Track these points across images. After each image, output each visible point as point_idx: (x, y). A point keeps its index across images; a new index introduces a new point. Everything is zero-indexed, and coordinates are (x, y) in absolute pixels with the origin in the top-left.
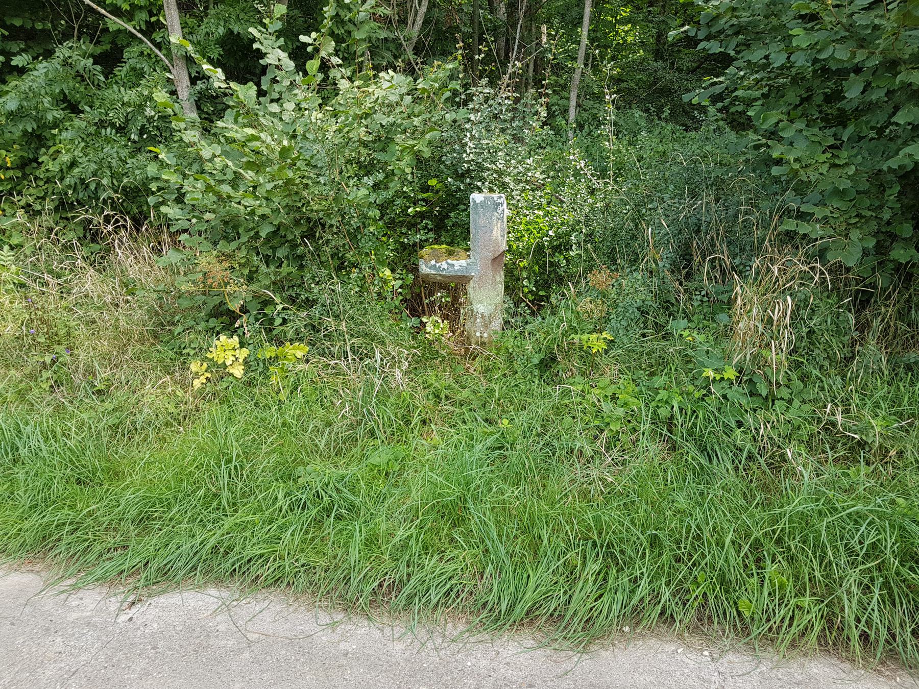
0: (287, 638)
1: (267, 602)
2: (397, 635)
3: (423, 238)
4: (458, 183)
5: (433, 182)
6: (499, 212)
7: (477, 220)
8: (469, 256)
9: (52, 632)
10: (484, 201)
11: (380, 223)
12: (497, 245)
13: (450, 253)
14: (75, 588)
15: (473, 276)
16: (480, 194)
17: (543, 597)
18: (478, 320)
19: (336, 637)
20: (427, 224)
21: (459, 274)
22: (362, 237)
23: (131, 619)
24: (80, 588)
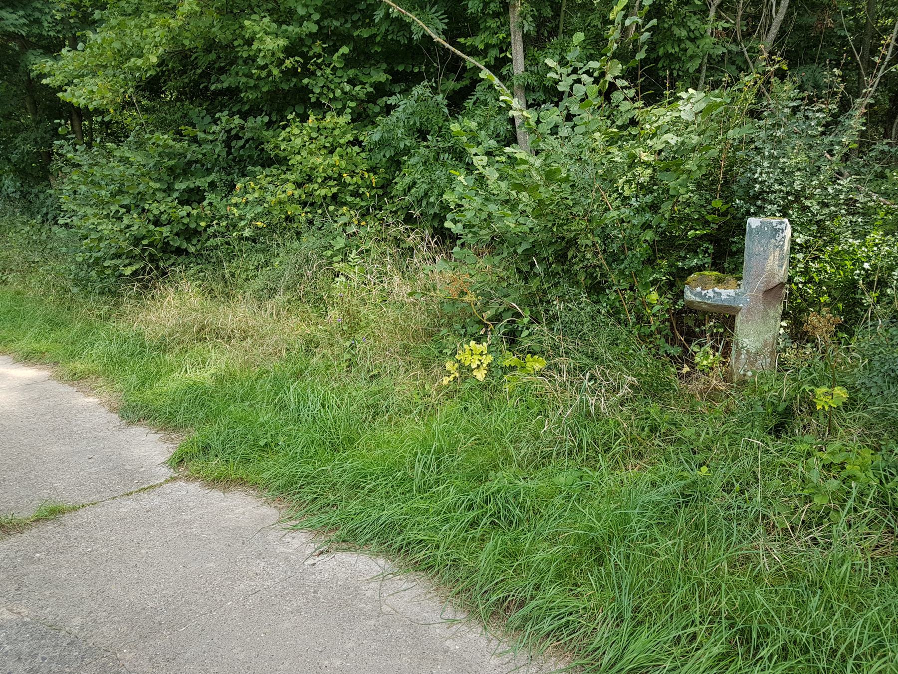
0: (410, 620)
1: (415, 583)
2: (500, 650)
6: (778, 239)
7: (751, 245)
8: (739, 285)
9: (261, 557)
10: (761, 226)
13: (719, 281)
14: (294, 529)
15: (741, 308)
16: (757, 219)
17: (653, 663)
18: (743, 356)
19: (448, 633)
20: (708, 248)
21: (726, 304)
23: (314, 564)
24: (297, 530)
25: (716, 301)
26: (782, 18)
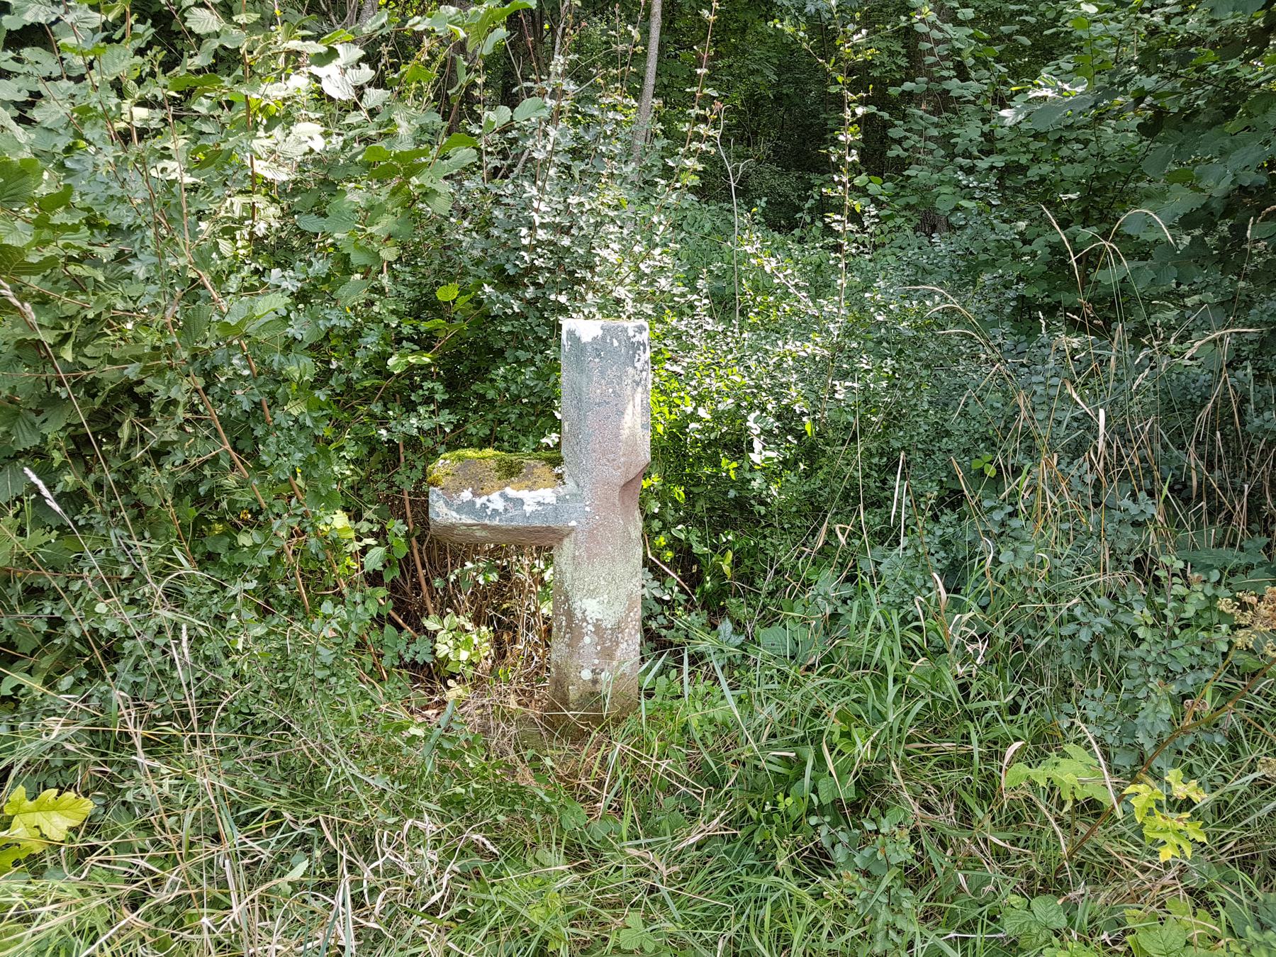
3: (427, 426)
4: (506, 297)
5: (447, 293)
8: (559, 476)
10: (603, 338)
11: (321, 395)
12: (633, 445)
13: (510, 471)
15: (573, 529)
18: (587, 640)
21: (537, 523)
22: (268, 433)
25: (512, 519)
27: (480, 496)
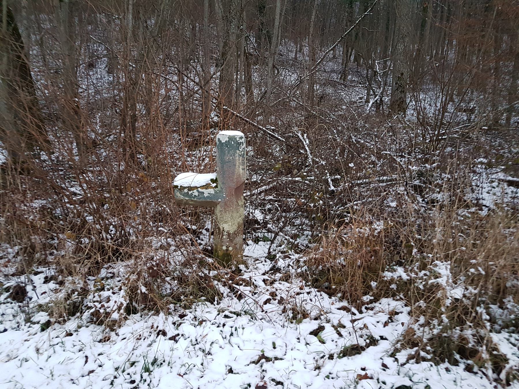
10: (229, 141)
21: (208, 200)
25: (200, 198)
26: (20, 31)
27: (190, 191)
